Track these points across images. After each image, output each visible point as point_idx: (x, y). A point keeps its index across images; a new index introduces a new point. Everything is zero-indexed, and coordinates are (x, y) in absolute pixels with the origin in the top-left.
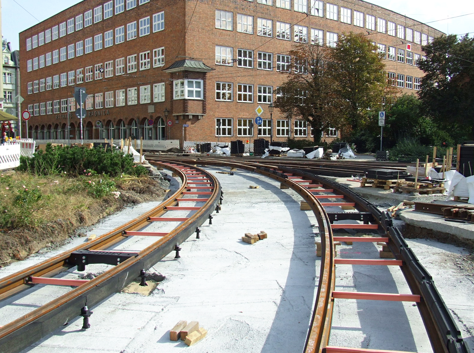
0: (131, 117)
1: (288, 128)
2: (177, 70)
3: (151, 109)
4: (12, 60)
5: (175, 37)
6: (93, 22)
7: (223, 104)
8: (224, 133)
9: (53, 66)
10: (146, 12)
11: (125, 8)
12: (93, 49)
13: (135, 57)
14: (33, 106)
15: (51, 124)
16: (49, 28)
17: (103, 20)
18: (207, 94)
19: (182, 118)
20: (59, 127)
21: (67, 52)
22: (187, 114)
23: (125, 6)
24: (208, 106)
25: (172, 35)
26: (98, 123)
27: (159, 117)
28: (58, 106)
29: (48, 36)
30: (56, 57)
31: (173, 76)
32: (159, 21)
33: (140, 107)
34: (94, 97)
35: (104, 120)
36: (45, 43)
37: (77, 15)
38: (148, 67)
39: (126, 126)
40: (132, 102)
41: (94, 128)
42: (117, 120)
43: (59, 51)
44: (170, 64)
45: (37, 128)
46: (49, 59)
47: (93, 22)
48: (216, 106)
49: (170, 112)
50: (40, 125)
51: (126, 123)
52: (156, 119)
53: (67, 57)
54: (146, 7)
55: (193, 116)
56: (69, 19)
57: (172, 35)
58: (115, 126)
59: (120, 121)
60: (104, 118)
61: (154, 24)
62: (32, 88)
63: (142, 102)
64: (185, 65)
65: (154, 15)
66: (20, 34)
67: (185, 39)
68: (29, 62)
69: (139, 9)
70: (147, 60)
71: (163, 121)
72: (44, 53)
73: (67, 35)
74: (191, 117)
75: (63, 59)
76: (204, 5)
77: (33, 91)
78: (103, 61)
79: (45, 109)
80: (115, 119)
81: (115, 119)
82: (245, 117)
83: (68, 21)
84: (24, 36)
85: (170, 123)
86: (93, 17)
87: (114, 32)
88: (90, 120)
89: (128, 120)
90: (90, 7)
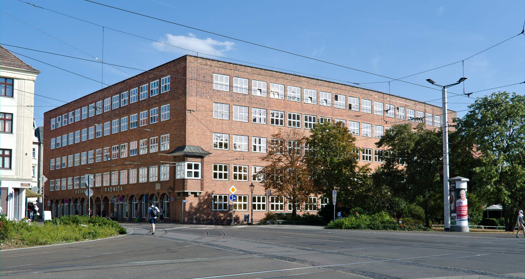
0: (142, 193)
1: (216, 202)
2: (179, 152)
3: (158, 187)
5: (178, 125)
6: (111, 109)
7: (220, 182)
8: (259, 208)
9: (75, 145)
10: (156, 103)
11: (139, 99)
12: (111, 132)
13: (157, 139)
15: (71, 198)
16: (117, 94)
17: (120, 108)
18: (205, 175)
19: (182, 194)
20: (78, 201)
21: (88, 133)
22: (186, 191)
23: (139, 97)
24: (205, 185)
25: (176, 124)
26: (113, 198)
27: (164, 194)
29: (86, 112)
30: (84, 135)
32: (165, 112)
33: (149, 184)
34: (110, 174)
35: (119, 196)
36: (88, 116)
37: (97, 101)
38: (146, 152)
39: (159, 200)
40: (143, 180)
41: (110, 202)
42: (130, 196)
43: (81, 132)
44: (174, 149)
46: (71, 139)
47: (111, 109)
48: (213, 184)
49: (173, 189)
50: (60, 199)
51: (138, 198)
52: (162, 196)
53: (88, 138)
54: (156, 99)
55: (192, 193)
56: (90, 103)
57: (176, 124)
58: (137, 201)
59: (132, 196)
60: (118, 193)
61: (162, 114)
62: (55, 163)
63: (151, 180)
64: (185, 150)
65: (162, 107)
66: (45, 113)
67: (185, 128)
68: (53, 140)
69: (150, 100)
70: (156, 144)
71: (168, 198)
72: (67, 132)
73: (88, 118)
74: (189, 194)
75: (84, 139)
76: (203, 100)
77: (55, 166)
78: (119, 143)
79: (65, 184)
80: (128, 195)
81: (128, 195)
82: (240, 193)
83: (162, 79)
85: (172, 199)
86: (111, 104)
87: (111, 123)
88: (107, 196)
89: (139, 196)
90: (109, 95)
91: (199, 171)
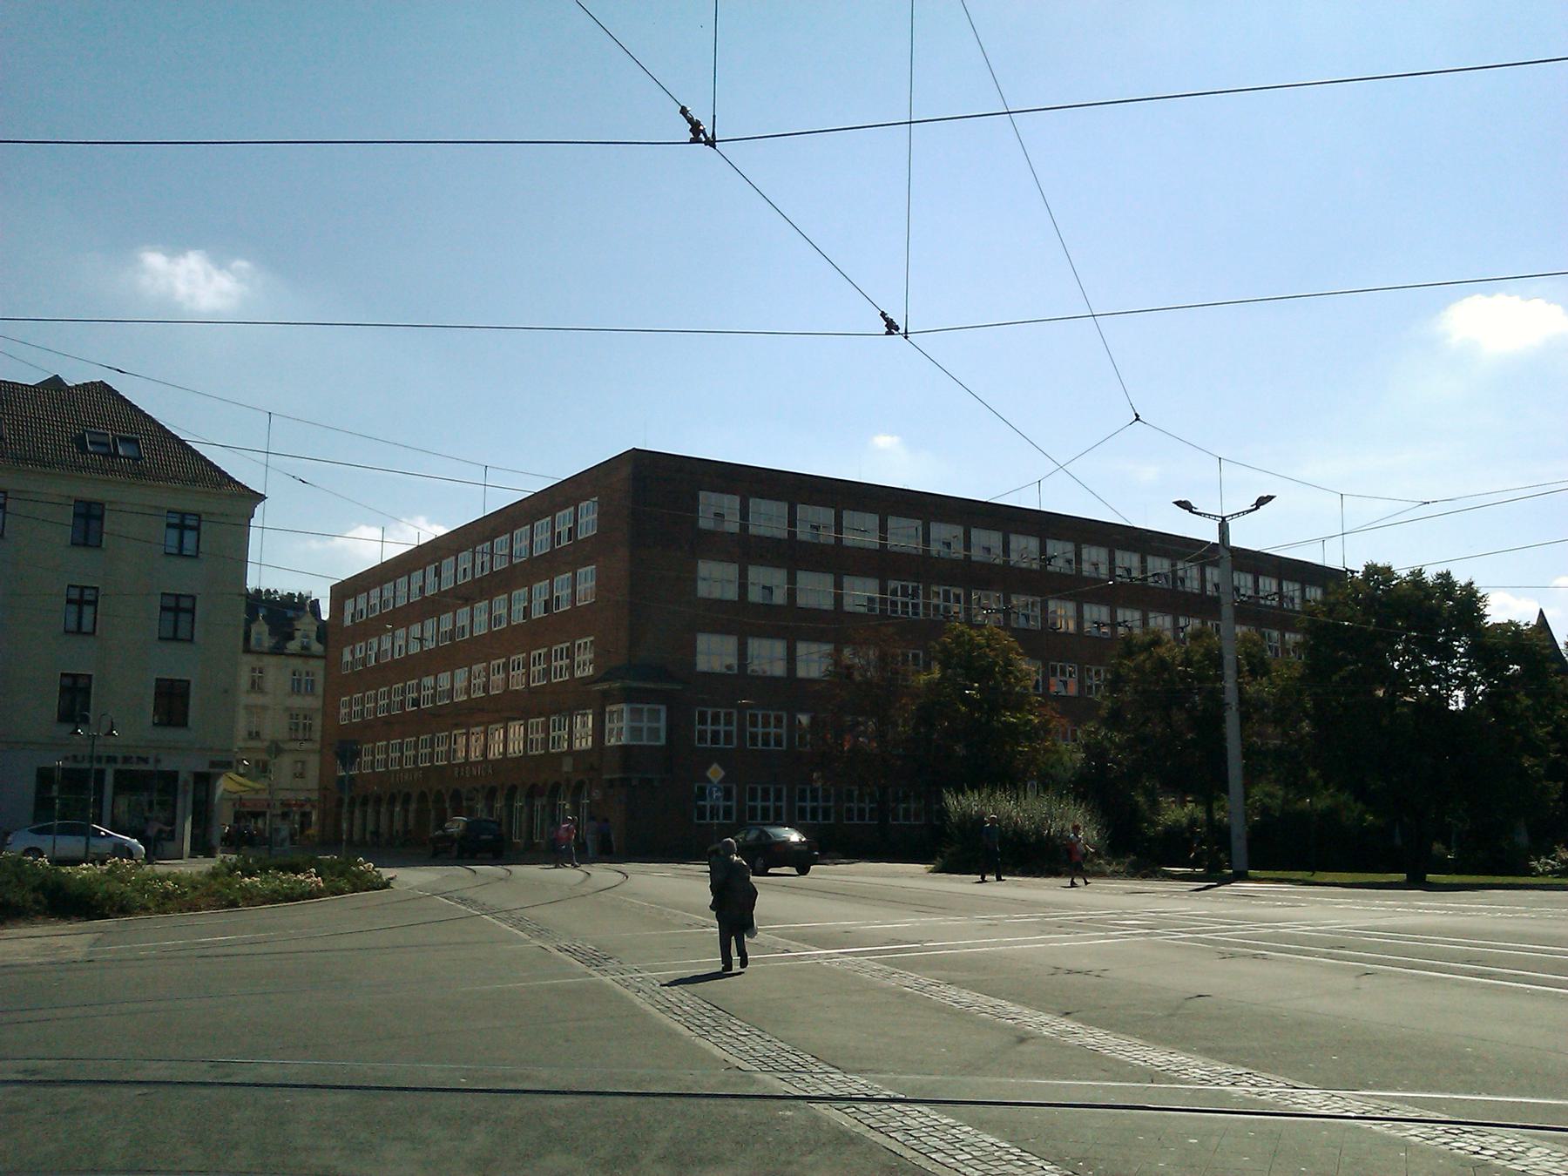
3: (567, 766)
4: (319, 639)
14: (401, 745)
28: (566, 662)
31: (607, 698)
45: (378, 800)
84: (342, 592)
91: (662, 724)
